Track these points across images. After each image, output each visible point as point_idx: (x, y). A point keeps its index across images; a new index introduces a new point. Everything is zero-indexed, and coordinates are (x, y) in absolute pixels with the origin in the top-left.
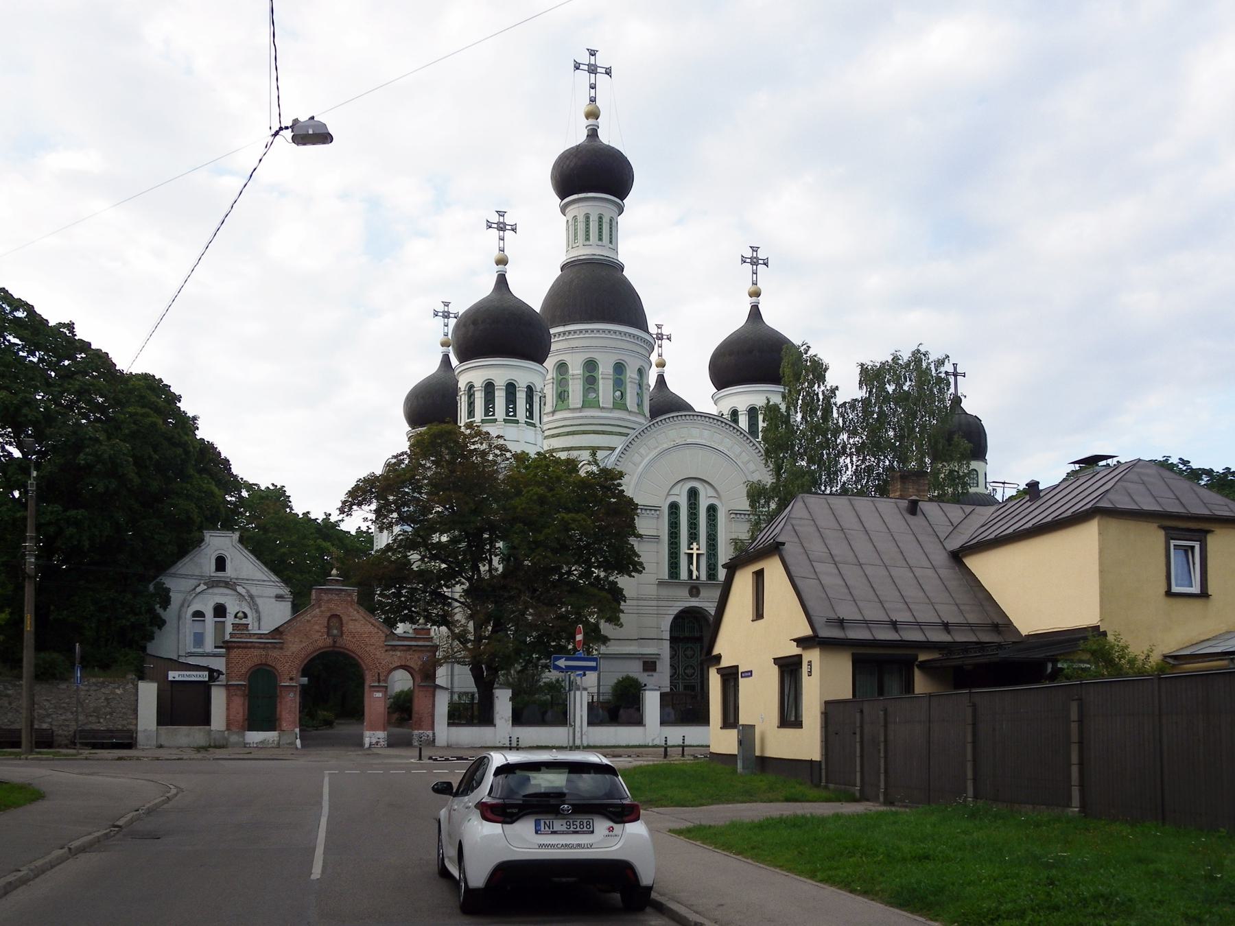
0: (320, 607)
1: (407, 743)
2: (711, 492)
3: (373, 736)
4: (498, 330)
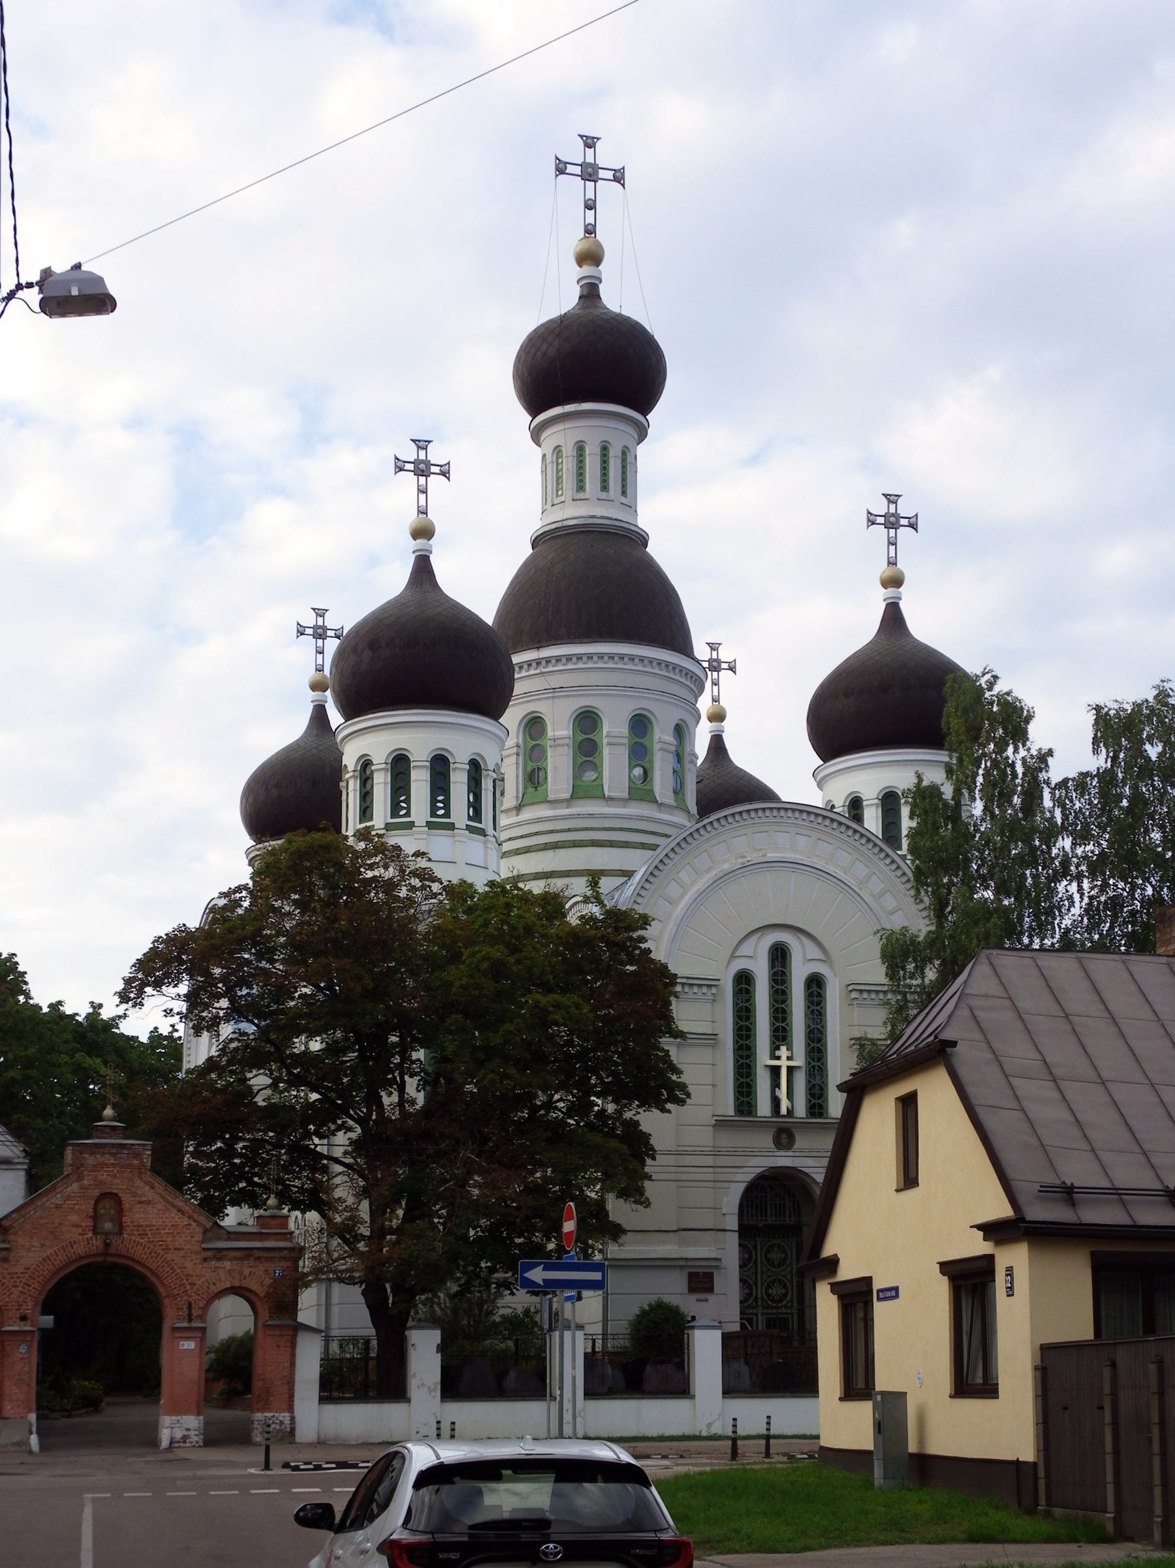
0: (80, 1178)
1: (239, 1437)
2: (813, 951)
3: (177, 1426)
4: (414, 658)
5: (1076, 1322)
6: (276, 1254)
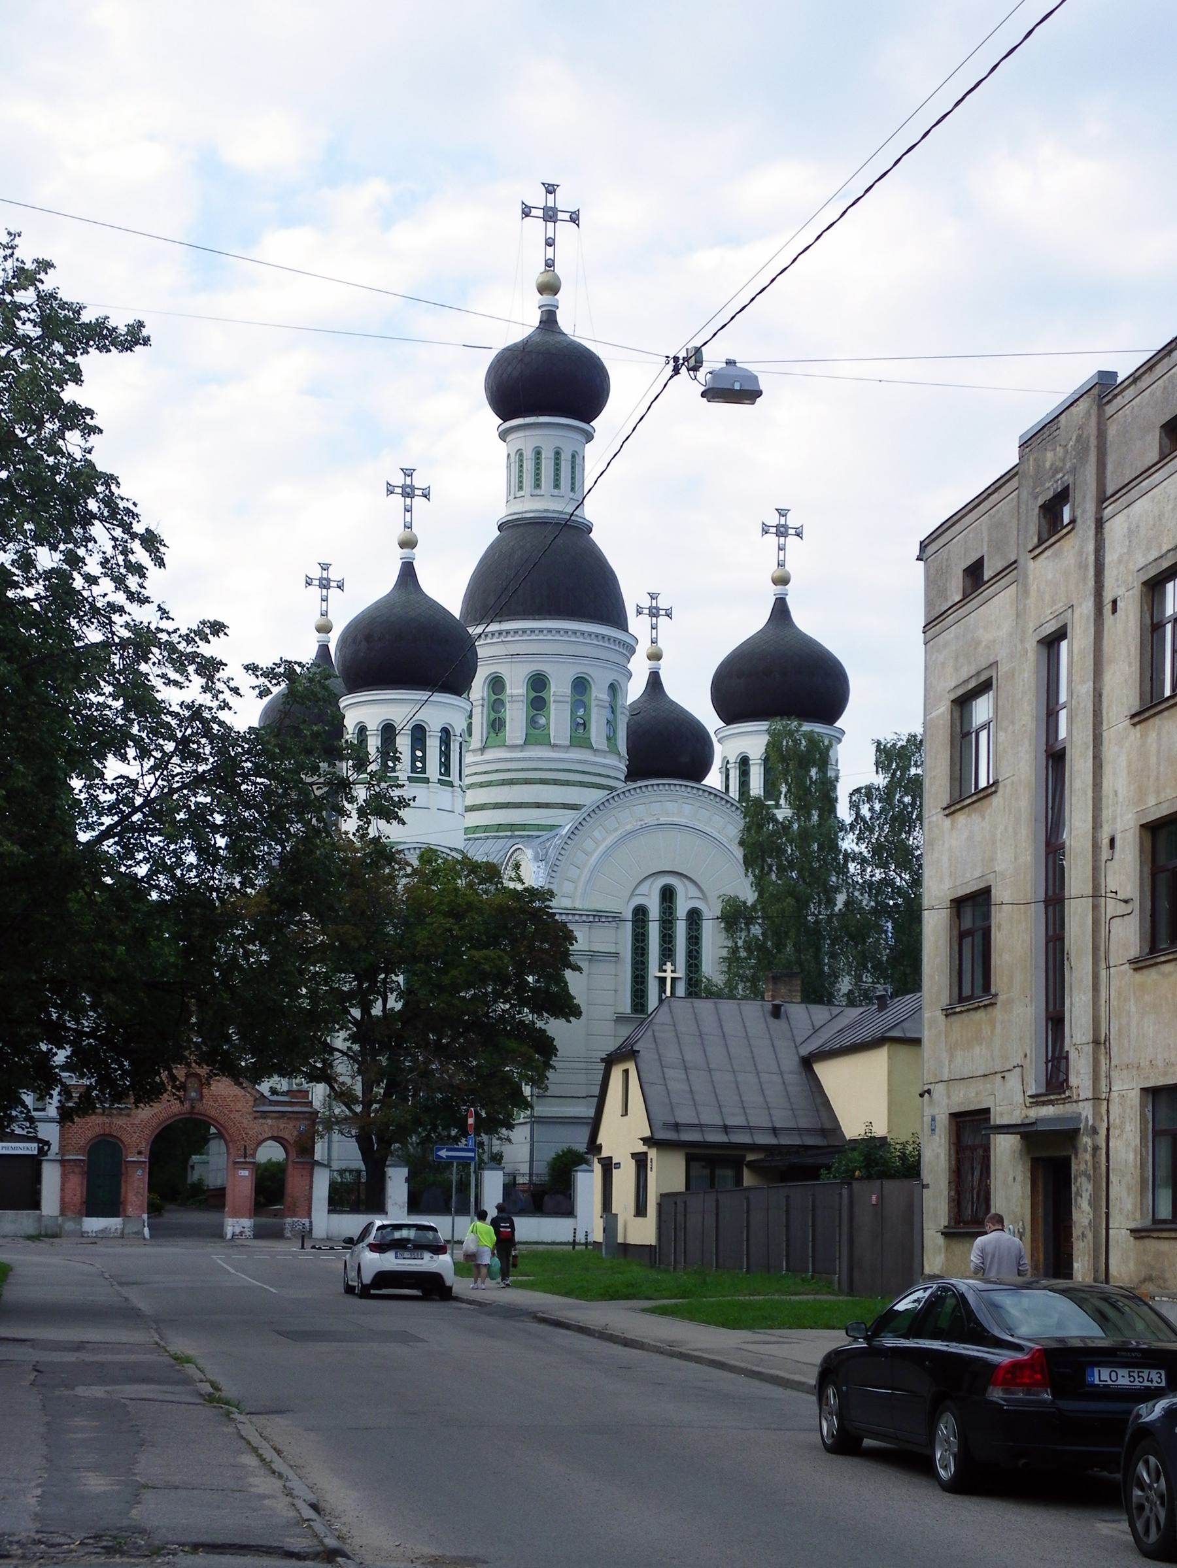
1: (277, 1234)
3: (237, 1225)
5: (678, 1184)
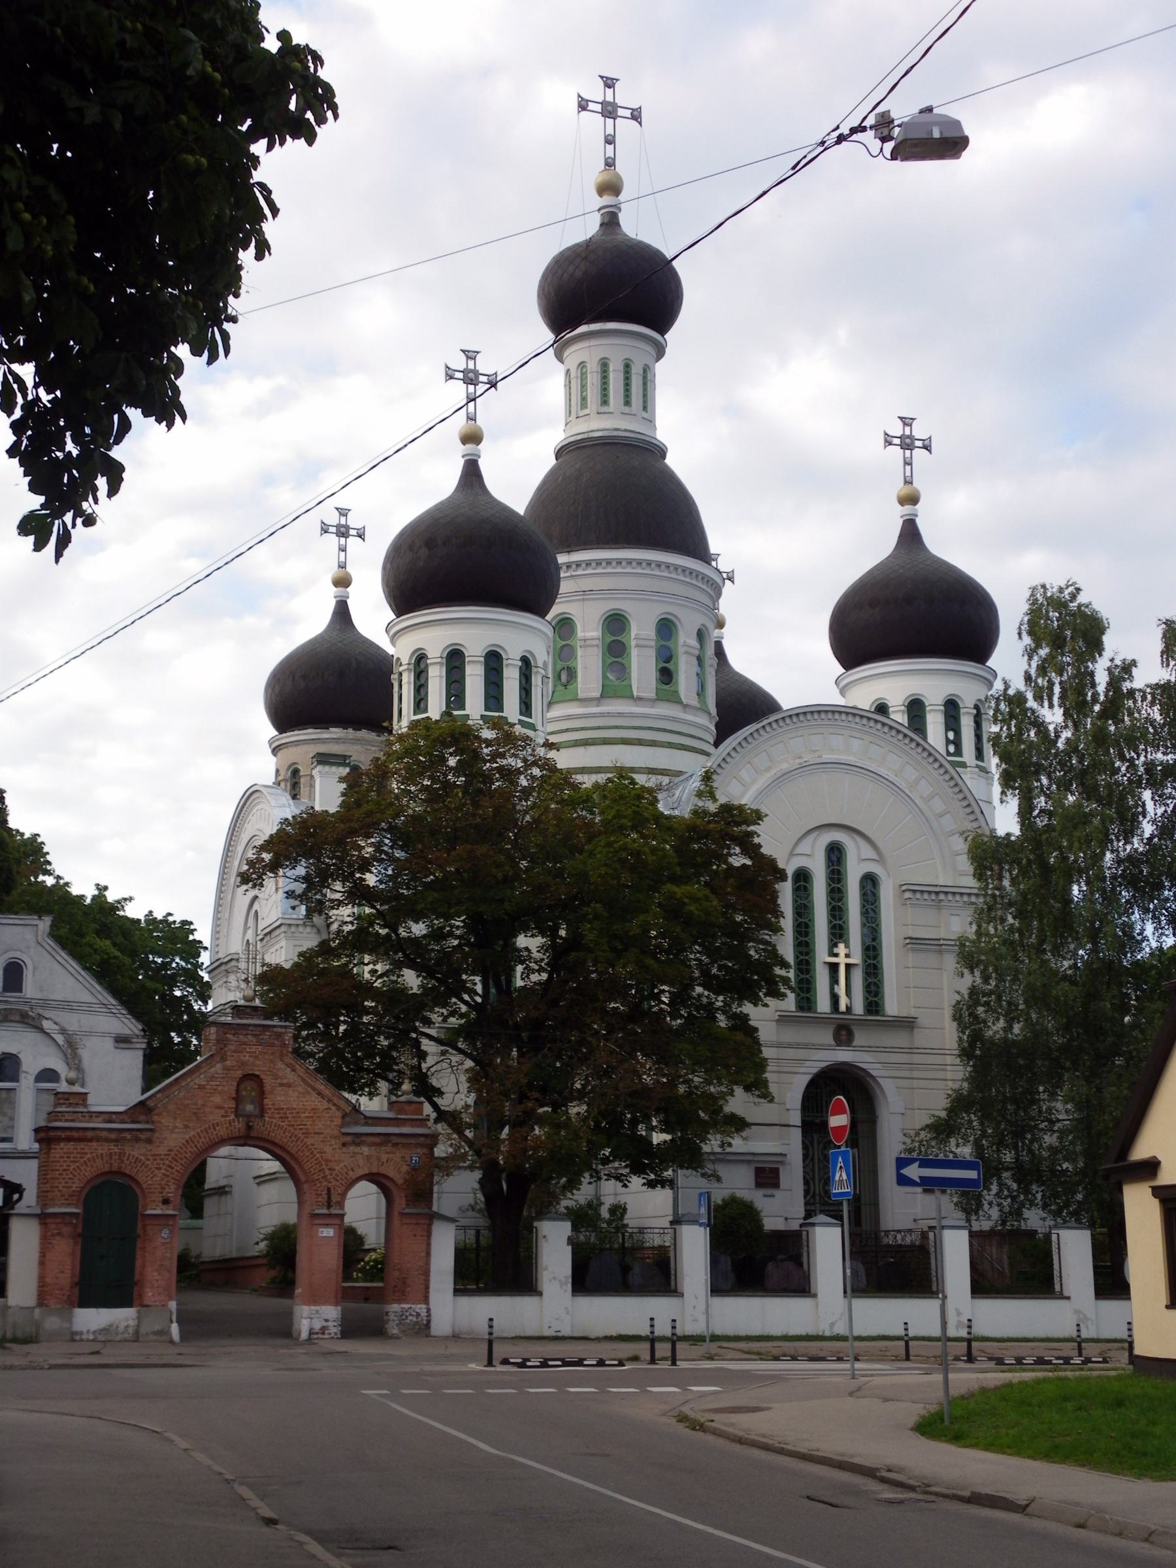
0: (223, 1059)
3: (315, 1317)
4: (463, 558)
6: (413, 1141)
